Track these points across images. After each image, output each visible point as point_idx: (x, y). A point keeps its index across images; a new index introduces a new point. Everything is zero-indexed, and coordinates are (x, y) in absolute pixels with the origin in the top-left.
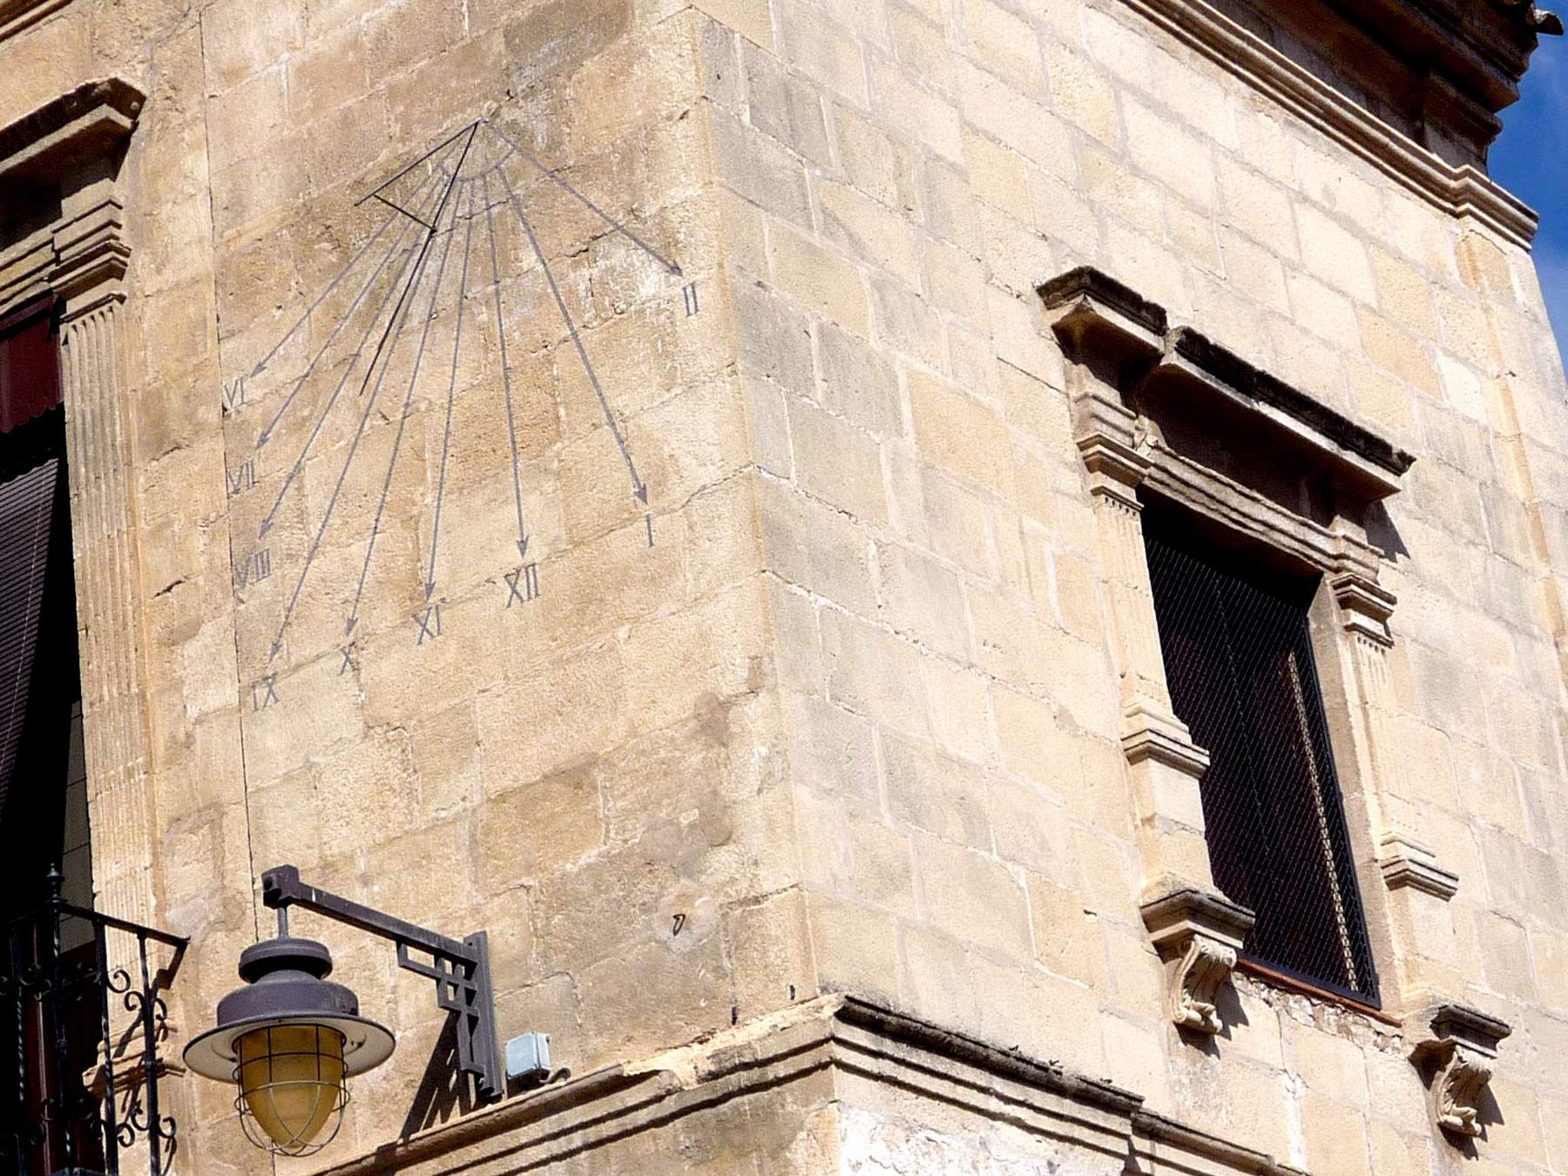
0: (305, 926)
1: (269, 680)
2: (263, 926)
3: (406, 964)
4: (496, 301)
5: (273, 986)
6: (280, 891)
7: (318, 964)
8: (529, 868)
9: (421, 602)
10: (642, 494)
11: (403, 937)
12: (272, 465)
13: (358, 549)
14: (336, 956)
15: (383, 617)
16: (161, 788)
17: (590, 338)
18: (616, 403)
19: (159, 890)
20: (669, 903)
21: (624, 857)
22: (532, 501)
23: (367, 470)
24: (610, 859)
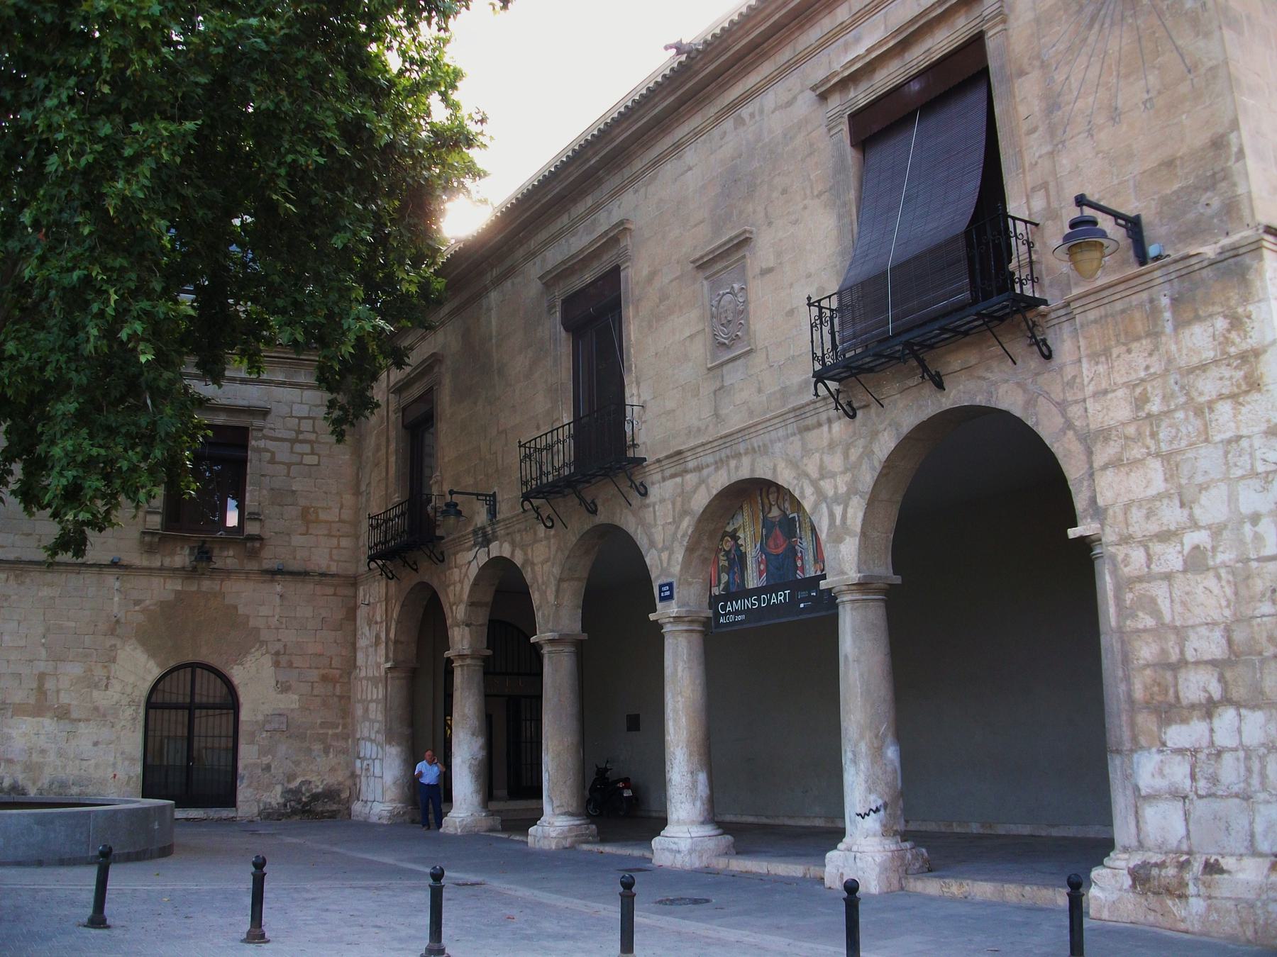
0: (1088, 212)
1: (1063, 142)
2: (1075, 213)
3: (1117, 224)
4: (1135, 16)
5: (828, 535)
6: (1081, 201)
7: (1095, 223)
8: (1155, 193)
9: (1115, 115)
10: (1189, 71)
11: (1116, 215)
12: (1059, 77)
13: (1091, 99)
14: (1099, 220)
15: (1100, 120)
16: (1028, 178)
17: (1168, 24)
18: (1180, 42)
19: (1029, 209)
20: (1204, 199)
21: (1188, 187)
22: (1151, 78)
23: (1093, 73)
24: (1182, 188)
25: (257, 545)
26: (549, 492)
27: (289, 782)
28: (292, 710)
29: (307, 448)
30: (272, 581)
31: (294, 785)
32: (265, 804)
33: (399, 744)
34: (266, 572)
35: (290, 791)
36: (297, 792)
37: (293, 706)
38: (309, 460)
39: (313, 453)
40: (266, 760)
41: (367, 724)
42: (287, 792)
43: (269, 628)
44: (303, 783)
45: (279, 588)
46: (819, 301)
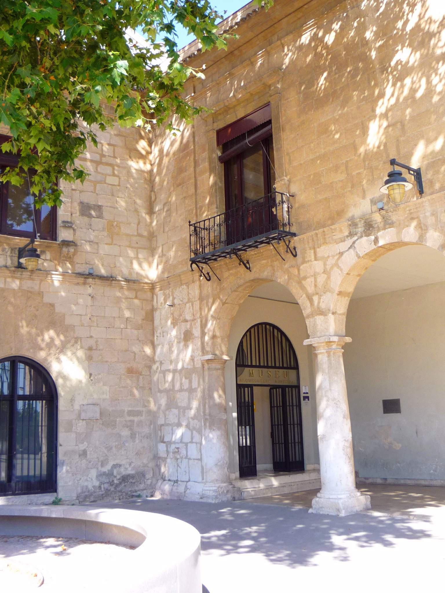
6: (393, 162)
7: (400, 174)
25: (72, 250)
26: (209, 259)
27: (102, 466)
28: (104, 400)
29: (108, 170)
30: (85, 284)
31: (107, 468)
32: (82, 487)
33: (219, 429)
34: (80, 274)
35: (104, 474)
36: (110, 474)
37: (104, 396)
38: (110, 180)
39: (114, 175)
40: (82, 447)
41: (175, 411)
42: (100, 475)
43: (83, 325)
44: (115, 466)
45: (90, 290)
46: (194, 224)
